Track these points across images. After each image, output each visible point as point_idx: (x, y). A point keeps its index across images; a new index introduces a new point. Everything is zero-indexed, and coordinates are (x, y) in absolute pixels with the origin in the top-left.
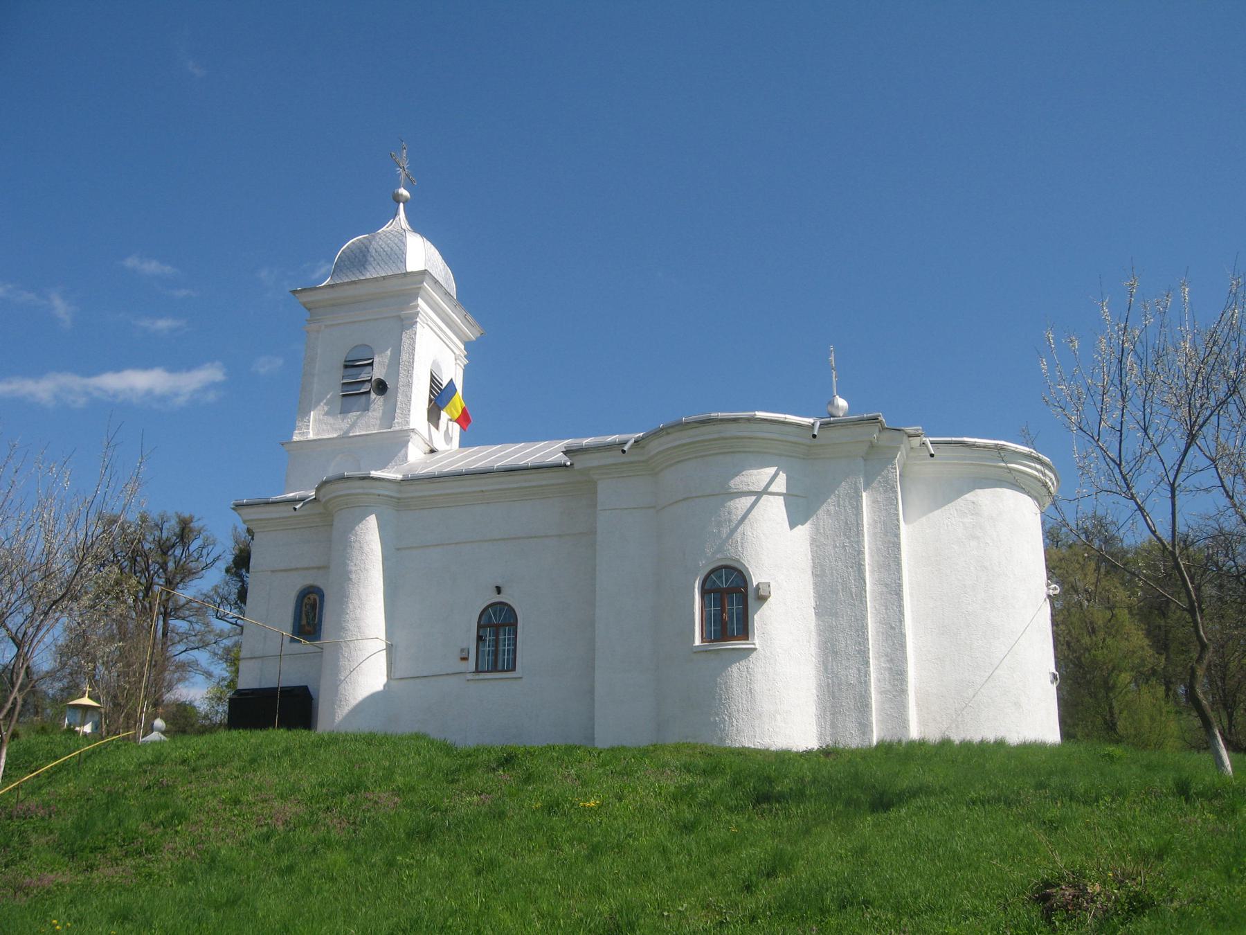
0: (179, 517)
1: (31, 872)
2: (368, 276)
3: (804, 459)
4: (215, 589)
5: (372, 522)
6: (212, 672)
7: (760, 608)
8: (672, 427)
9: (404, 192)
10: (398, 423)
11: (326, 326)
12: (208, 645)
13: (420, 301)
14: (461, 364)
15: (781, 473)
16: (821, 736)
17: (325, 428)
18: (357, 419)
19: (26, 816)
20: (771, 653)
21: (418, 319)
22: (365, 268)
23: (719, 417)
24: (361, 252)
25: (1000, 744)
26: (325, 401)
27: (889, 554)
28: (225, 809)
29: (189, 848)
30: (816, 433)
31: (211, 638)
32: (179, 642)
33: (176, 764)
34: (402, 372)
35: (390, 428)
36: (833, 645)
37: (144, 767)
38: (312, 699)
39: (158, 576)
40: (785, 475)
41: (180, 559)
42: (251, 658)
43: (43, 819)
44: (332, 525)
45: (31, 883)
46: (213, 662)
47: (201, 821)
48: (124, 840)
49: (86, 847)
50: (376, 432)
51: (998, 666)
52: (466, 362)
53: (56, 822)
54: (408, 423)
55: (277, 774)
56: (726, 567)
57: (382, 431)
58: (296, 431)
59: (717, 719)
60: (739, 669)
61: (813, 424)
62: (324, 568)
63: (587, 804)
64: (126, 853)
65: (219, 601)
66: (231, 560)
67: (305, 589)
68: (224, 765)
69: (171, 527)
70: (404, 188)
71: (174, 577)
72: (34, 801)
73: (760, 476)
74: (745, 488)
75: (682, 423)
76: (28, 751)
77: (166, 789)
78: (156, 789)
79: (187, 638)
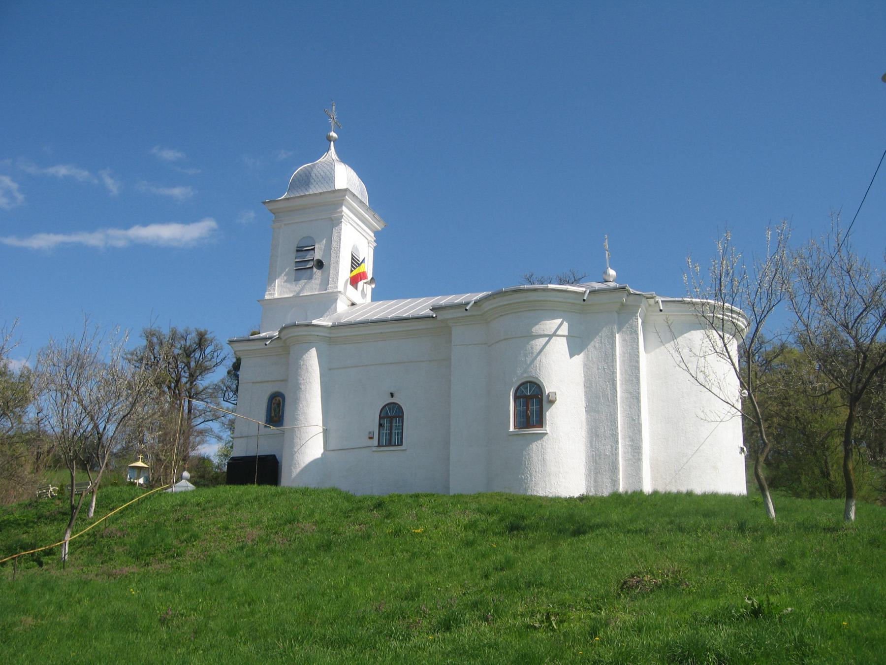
0: (197, 331)
1: (116, 566)
2: (311, 192)
3: (580, 313)
4: (222, 381)
5: (313, 352)
6: (222, 436)
7: (550, 408)
8: (497, 294)
9: (333, 134)
10: (331, 287)
11: (285, 224)
12: (218, 418)
13: (344, 208)
14: (372, 246)
15: (565, 322)
16: (588, 488)
17: (285, 290)
18: (305, 285)
19: (110, 536)
20: (556, 436)
21: (343, 220)
22: (309, 187)
23: (526, 288)
24: (306, 176)
25: (690, 494)
26: (285, 273)
27: (632, 373)
28: (220, 532)
29: (199, 554)
30: (585, 298)
31: (220, 413)
32: (199, 416)
33: (193, 506)
34: (333, 255)
35: (326, 290)
36: (596, 430)
37: (176, 507)
38: (278, 463)
39: (185, 372)
40: (567, 324)
41: (199, 360)
42: (241, 437)
43: (120, 538)
44: (289, 354)
45: (116, 572)
46: (222, 430)
47: (207, 539)
48: (165, 550)
49: (144, 553)
50: (316, 293)
51: (703, 443)
52: (375, 244)
53: (127, 540)
54: (337, 287)
55: (250, 512)
56: (530, 382)
57: (322, 292)
58: (267, 293)
59: (523, 476)
60: (537, 446)
61: (585, 292)
62: (285, 381)
63: (416, 531)
64: (166, 557)
65: (225, 389)
66: (231, 365)
67: (273, 394)
68: (220, 507)
69: (192, 338)
70: (334, 132)
71: (195, 372)
72: (113, 527)
73: (551, 325)
74: (542, 333)
76: (107, 497)
77: (188, 521)
78: (182, 521)
79: (204, 413)
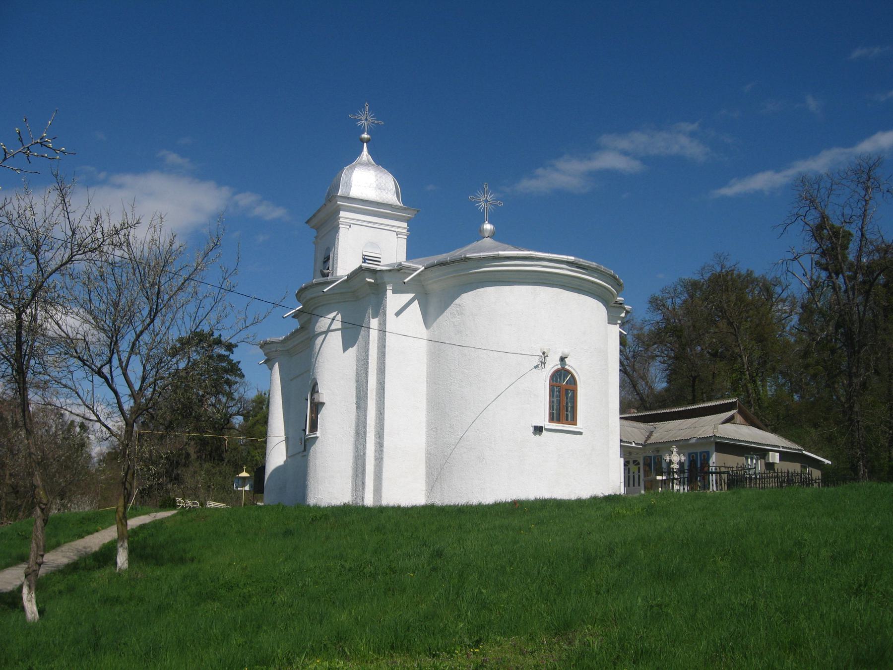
5: (277, 363)
75: (303, 289)
